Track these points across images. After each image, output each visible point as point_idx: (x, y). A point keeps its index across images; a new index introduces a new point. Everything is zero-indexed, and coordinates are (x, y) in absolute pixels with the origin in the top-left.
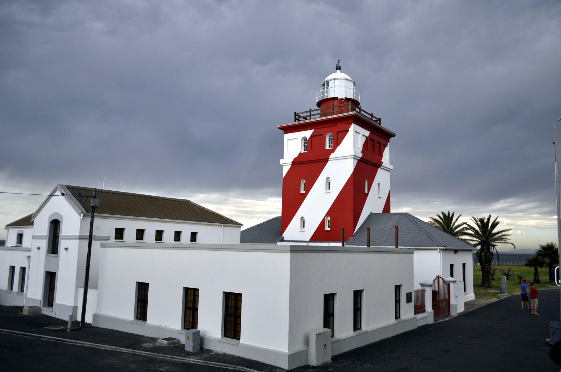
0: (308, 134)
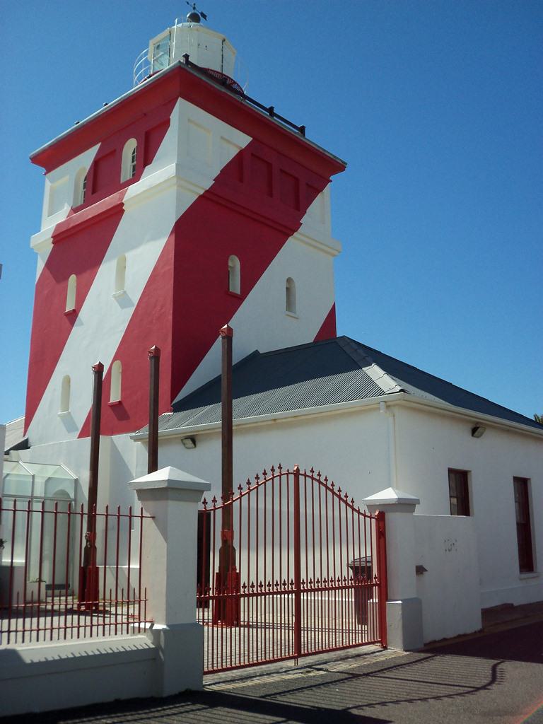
0: (87, 158)
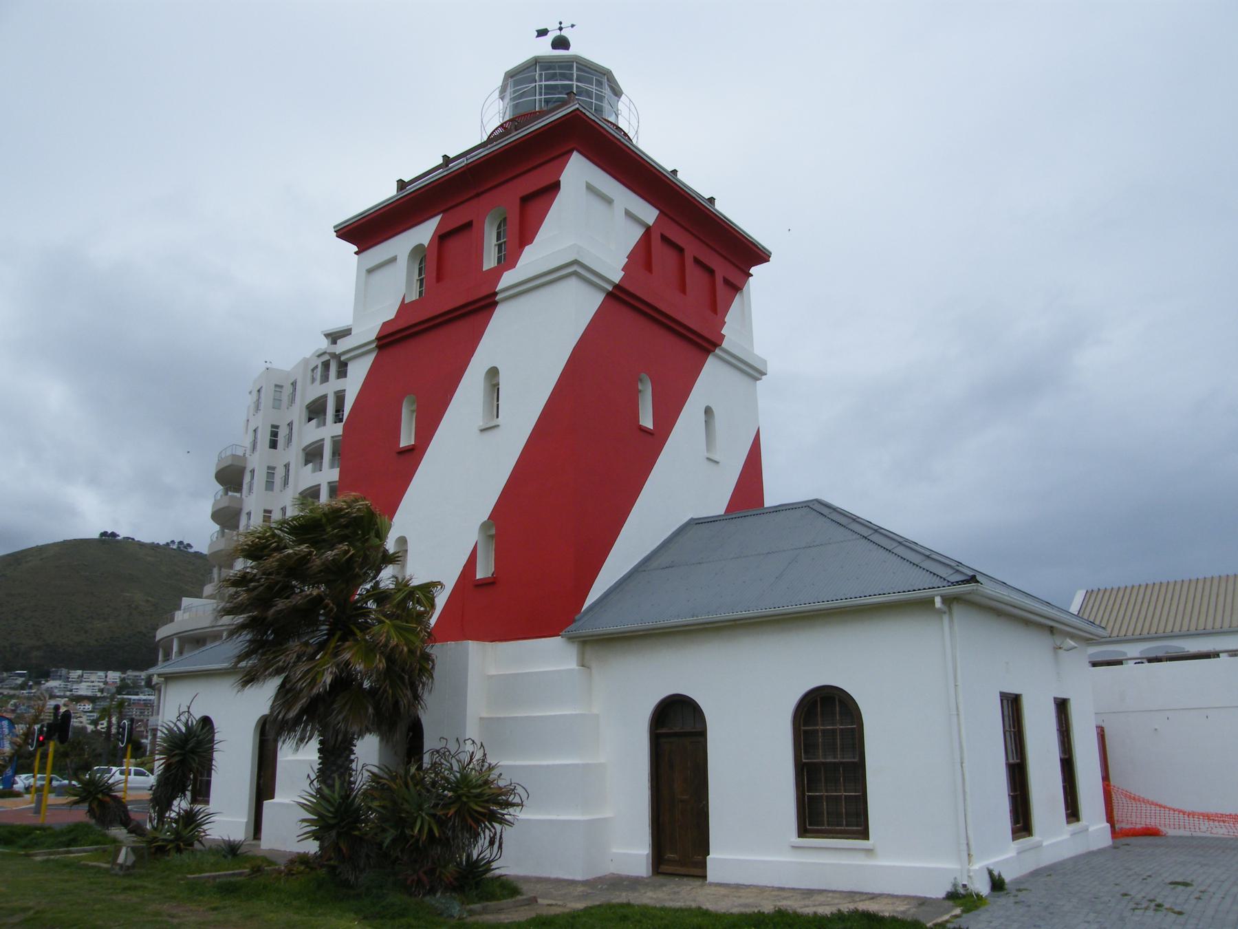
0: (424, 233)
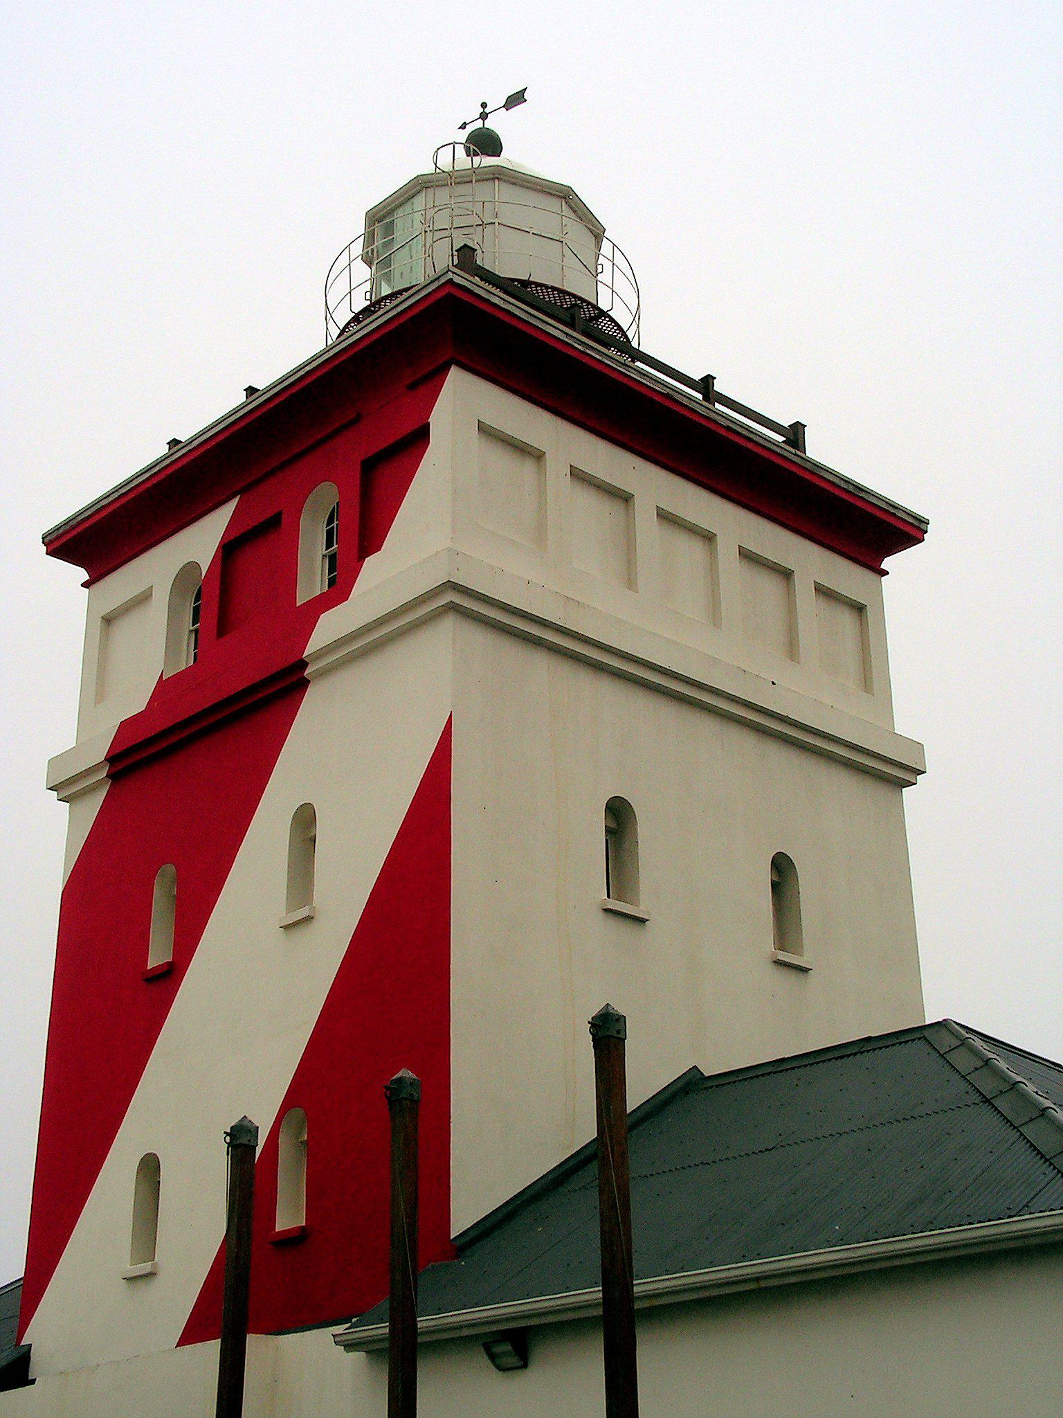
0: (200, 543)
